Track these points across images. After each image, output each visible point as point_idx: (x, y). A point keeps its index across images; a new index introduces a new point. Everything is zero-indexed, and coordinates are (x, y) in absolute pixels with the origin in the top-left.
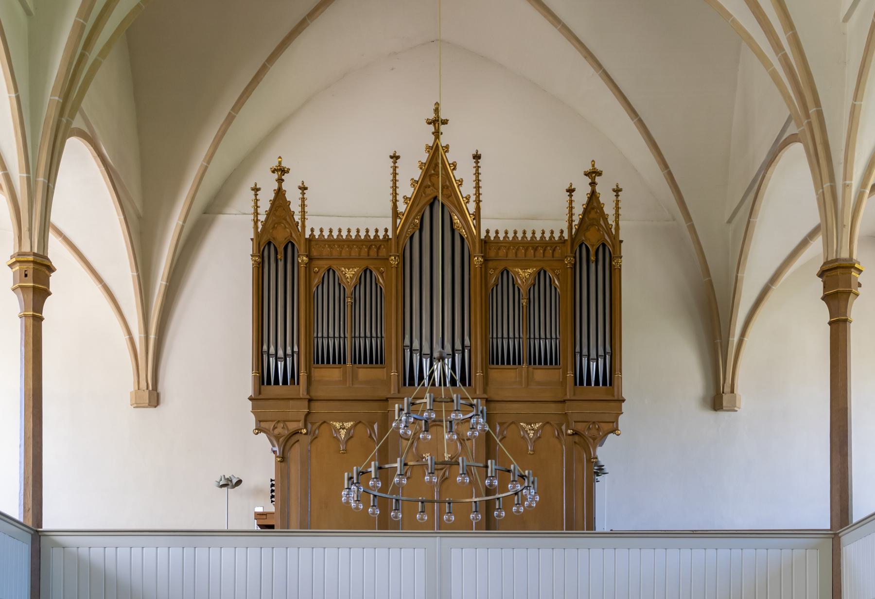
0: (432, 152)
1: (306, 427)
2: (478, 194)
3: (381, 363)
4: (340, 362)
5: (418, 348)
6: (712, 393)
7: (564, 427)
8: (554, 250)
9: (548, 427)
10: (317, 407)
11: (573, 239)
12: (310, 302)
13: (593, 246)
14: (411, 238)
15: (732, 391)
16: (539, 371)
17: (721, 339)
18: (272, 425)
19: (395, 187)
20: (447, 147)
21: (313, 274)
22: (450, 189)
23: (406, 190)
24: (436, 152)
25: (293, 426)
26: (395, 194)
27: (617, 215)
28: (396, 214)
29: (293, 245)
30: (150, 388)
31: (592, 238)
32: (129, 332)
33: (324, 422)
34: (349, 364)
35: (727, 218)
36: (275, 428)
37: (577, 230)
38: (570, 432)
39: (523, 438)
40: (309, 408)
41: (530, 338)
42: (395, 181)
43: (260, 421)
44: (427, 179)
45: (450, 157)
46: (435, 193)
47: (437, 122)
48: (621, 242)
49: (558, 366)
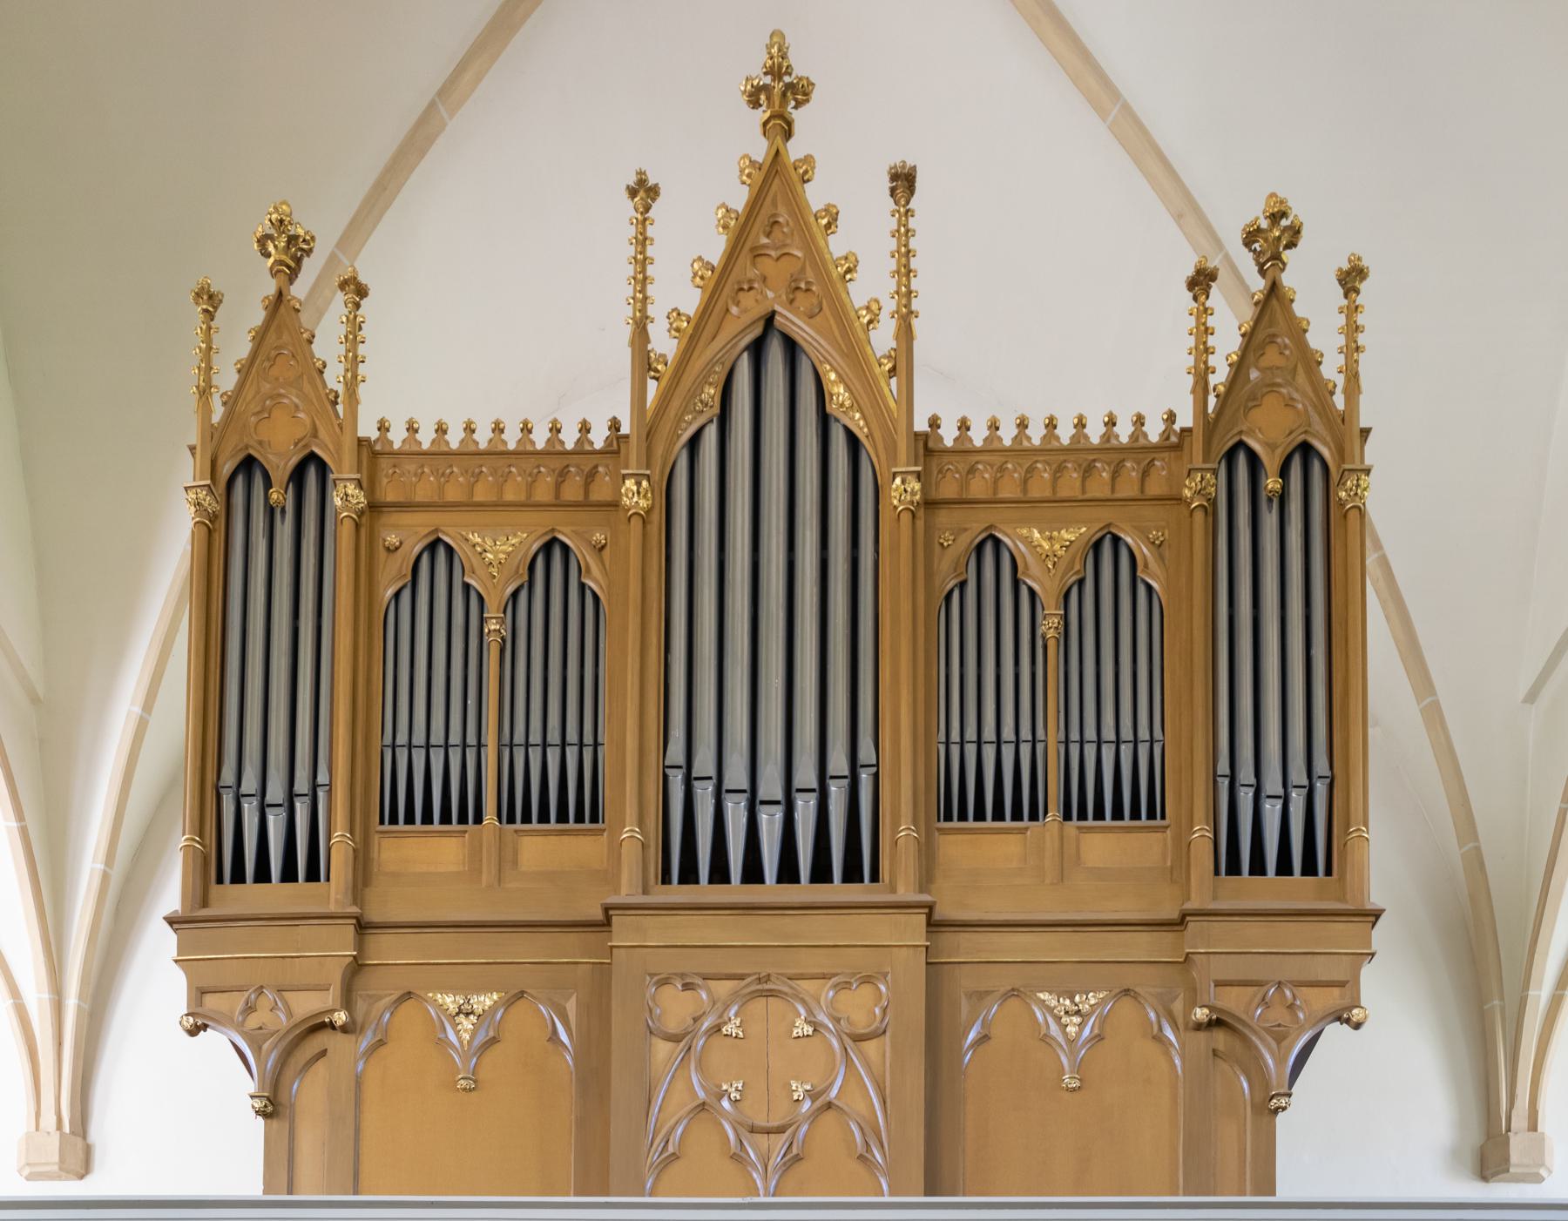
0: (759, 177)
1: (347, 1003)
2: (906, 295)
3: (594, 819)
4: (463, 819)
5: (711, 771)
6: (1475, 1137)
7: (1178, 1006)
8: (1145, 474)
9: (1127, 1002)
10: (385, 949)
11: (1210, 425)
12: (370, 637)
13: (1272, 447)
14: (694, 443)
15: (1533, 1127)
16: (1096, 839)
17: (1502, 999)
18: (239, 1001)
19: (642, 281)
20: (808, 159)
21: (382, 553)
22: (821, 283)
23: (678, 293)
24: (776, 182)
25: (307, 1005)
26: (642, 302)
27: (1352, 349)
28: (644, 363)
29: (323, 468)
30: (67, 1129)
31: (1268, 435)
32: (14, 992)
33: (408, 995)
34: (489, 816)
35: (1523, 688)
36: (249, 1009)
37: (1224, 400)
38: (1201, 1014)
39: (1046, 1039)
40: (360, 945)
41: (1067, 742)
42: (642, 262)
43: (203, 992)
44: (744, 259)
45: (816, 196)
46: (768, 352)
47: (780, 94)
48: (1365, 433)
49: (1158, 822)
